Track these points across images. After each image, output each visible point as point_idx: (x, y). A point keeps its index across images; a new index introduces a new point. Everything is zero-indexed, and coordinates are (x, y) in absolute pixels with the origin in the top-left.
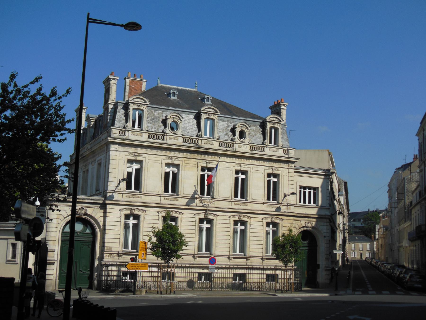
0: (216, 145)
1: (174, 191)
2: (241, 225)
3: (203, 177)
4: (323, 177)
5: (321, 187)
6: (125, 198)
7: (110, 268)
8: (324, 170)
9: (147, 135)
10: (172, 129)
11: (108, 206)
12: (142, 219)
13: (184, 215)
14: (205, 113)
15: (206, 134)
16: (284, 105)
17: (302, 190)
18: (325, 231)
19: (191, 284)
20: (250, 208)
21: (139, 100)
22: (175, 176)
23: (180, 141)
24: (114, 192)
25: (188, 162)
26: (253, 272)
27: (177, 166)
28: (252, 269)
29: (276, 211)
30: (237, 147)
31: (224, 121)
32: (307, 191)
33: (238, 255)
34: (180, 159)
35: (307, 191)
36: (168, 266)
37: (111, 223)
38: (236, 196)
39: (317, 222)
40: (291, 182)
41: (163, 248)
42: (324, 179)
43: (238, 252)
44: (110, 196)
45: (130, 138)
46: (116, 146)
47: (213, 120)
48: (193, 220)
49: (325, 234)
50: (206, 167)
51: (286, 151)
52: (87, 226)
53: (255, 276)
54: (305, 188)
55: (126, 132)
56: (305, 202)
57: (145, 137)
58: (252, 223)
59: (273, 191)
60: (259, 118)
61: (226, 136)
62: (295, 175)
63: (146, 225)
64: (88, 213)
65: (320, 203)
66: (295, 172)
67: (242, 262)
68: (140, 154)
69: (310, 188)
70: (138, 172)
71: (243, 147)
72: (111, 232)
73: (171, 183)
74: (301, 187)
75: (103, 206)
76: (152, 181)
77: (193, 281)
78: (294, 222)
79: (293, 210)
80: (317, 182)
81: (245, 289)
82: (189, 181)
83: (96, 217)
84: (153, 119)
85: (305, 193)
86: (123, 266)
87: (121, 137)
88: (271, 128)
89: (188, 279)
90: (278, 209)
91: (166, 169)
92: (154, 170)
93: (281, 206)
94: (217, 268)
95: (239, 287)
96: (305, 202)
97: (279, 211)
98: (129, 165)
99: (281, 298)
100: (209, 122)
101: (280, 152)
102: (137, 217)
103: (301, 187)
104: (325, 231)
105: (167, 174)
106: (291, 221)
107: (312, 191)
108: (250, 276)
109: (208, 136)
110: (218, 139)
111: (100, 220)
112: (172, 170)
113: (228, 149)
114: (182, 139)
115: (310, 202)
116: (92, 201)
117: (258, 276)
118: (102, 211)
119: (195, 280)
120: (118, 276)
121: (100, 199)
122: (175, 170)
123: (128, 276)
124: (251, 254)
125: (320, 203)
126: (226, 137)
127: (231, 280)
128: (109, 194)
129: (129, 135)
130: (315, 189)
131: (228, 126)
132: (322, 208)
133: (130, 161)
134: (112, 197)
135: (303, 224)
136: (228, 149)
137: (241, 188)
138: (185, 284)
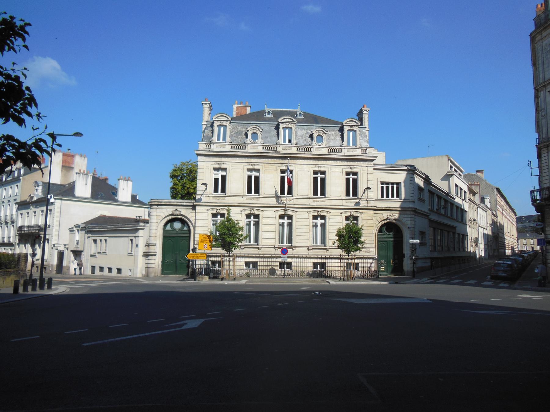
0: (294, 150)
2: (254, 218)
4: (406, 172)
5: (404, 182)
6: (211, 200)
7: (237, 259)
8: (406, 166)
9: (230, 146)
10: (318, 141)
11: (197, 207)
12: (260, 217)
13: (265, 212)
15: (349, 144)
16: (366, 110)
17: (385, 186)
18: (409, 222)
19: (272, 272)
21: (222, 117)
22: (323, 180)
23: (260, 149)
24: (202, 195)
25: (267, 166)
27: (258, 170)
29: (355, 206)
30: (314, 151)
31: (303, 129)
32: (390, 186)
33: (319, 246)
34: (260, 164)
35: (390, 186)
36: (229, 256)
37: (200, 221)
38: (382, 196)
39: (400, 214)
40: (370, 179)
41: (223, 239)
42: (407, 174)
43: (319, 244)
44: (199, 199)
45: (215, 150)
46: (203, 157)
47: (355, 131)
48: (274, 216)
49: (409, 226)
50: (351, 172)
51: (365, 151)
52: (184, 225)
54: (387, 183)
55: (212, 145)
56: (387, 196)
57: (228, 148)
58: (331, 217)
59: (352, 187)
60: (336, 123)
61: (304, 141)
62: (374, 173)
64: (182, 213)
65: (403, 196)
66: (374, 169)
67: (321, 252)
68: (224, 163)
69: (393, 184)
70: (224, 178)
71: (321, 150)
72: (200, 228)
73: (253, 185)
74: (382, 183)
75: (194, 207)
76: (237, 183)
77: (274, 270)
78: (375, 215)
79: (372, 204)
80: (400, 177)
81: (325, 277)
82: (270, 181)
83: (189, 217)
84: (237, 133)
85: (387, 188)
87: (207, 149)
89: (270, 267)
90: (358, 204)
91: (249, 174)
92: (237, 175)
93: (360, 201)
94: (288, 257)
95: (320, 275)
96: (387, 196)
97: (359, 206)
98: (216, 172)
99: (333, 286)
100: (287, 131)
101: (359, 152)
102: (323, 218)
103: (382, 183)
104: (409, 222)
105: (250, 178)
106: (371, 215)
107: (395, 186)
108: (330, 265)
109: (351, 145)
110: (296, 144)
111: (192, 219)
112: (254, 174)
113: (306, 153)
114: (262, 147)
115: (393, 196)
116: (185, 204)
118: (194, 211)
119: (277, 268)
120: (207, 265)
121: (191, 202)
122: (257, 174)
123: (217, 264)
124: (297, 245)
125: (403, 196)
126: (305, 142)
127: (311, 268)
128: (197, 198)
129: (214, 147)
130: (398, 184)
131: (307, 133)
132: (405, 201)
133: (216, 169)
134: (200, 200)
135: (385, 216)
136: (306, 153)
137: (320, 186)
138: (267, 272)
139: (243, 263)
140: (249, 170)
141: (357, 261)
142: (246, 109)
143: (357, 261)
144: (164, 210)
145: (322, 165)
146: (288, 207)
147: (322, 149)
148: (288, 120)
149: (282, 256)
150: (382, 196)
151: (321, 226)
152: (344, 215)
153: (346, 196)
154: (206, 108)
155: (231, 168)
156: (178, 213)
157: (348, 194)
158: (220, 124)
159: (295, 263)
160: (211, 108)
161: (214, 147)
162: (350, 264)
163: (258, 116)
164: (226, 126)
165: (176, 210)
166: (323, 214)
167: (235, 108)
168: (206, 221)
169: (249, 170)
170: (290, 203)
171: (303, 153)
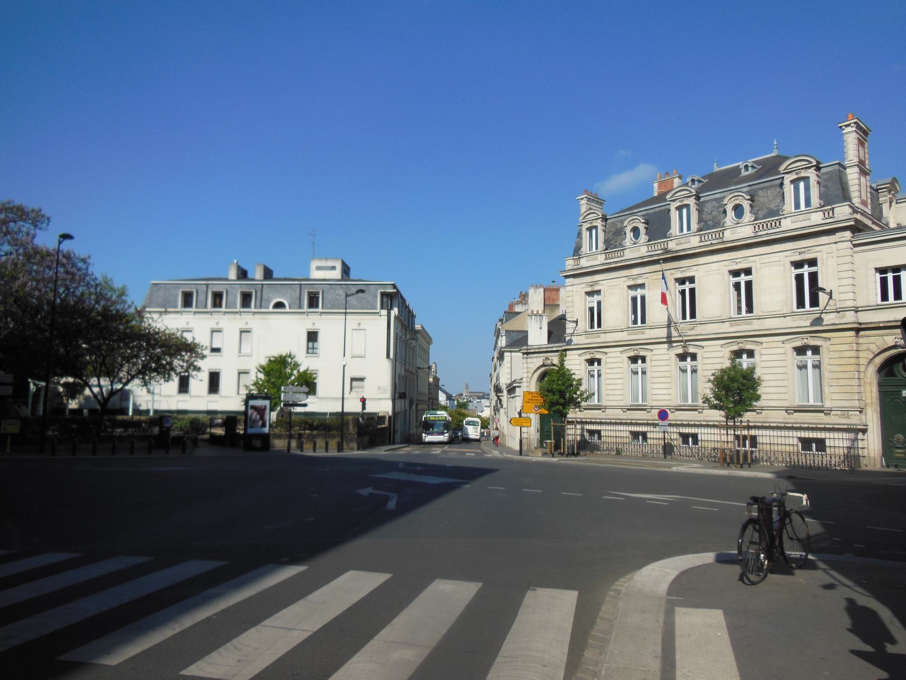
1: (599, 326)
3: (799, 278)
13: (654, 352)
14: (673, 201)
20: (757, 328)
24: (572, 334)
26: (772, 433)
28: (708, 426)
29: (812, 325)
32: (890, 276)
38: (885, 297)
53: (619, 434)
58: (764, 352)
63: (608, 371)
66: (855, 246)
68: (596, 283)
74: (882, 271)
86: (586, 423)
88: (679, 209)
90: (818, 321)
91: (632, 293)
92: (615, 296)
93: (823, 316)
94: (670, 425)
98: (589, 299)
108: (705, 437)
112: (593, 301)
113: (714, 242)
117: (783, 441)
120: (582, 435)
123: (814, 445)
128: (568, 339)
133: (589, 294)
139: (628, 434)
140: (630, 287)
141: (753, 432)
142: (672, 183)
143: (753, 432)
144: (534, 360)
145: (740, 259)
146: (687, 341)
147: (743, 229)
148: (682, 193)
149: (661, 423)
150: (885, 297)
151: (814, 367)
152: (789, 346)
153: (798, 308)
154: (851, 138)
155: (825, 256)
156: (549, 362)
157: (801, 303)
158: (795, 177)
159: (764, 437)
160: (863, 133)
161: (584, 262)
162: (745, 437)
163: (727, 179)
164: (808, 178)
165: (547, 358)
166: (749, 347)
167: (656, 185)
168: (783, 357)
169: (630, 287)
170: (692, 332)
171: (709, 243)
